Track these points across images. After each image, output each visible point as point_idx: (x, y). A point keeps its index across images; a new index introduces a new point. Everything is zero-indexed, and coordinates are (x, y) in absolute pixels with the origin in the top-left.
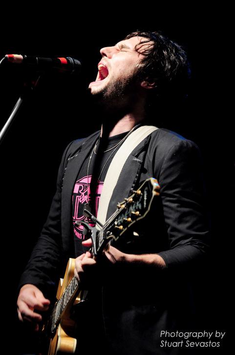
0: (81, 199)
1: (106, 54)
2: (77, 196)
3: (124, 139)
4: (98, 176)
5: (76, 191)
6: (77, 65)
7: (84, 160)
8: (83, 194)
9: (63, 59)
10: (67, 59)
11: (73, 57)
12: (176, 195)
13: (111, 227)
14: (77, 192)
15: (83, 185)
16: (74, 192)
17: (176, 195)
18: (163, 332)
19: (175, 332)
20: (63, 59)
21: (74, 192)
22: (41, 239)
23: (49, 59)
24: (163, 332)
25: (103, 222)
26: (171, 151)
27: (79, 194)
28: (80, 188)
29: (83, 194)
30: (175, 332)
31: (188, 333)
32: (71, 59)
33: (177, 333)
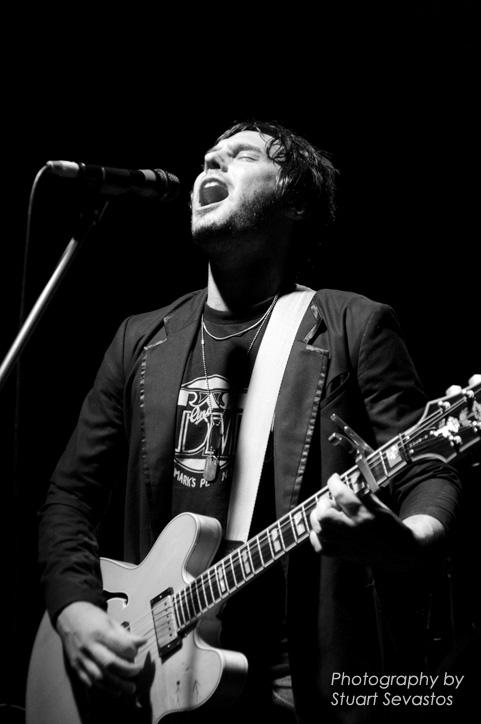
0: (192, 416)
1: (221, 164)
2: (185, 412)
3: (268, 311)
4: (238, 370)
5: (182, 400)
6: (174, 182)
7: (188, 356)
8: (197, 407)
9: (148, 173)
10: (156, 173)
11: (168, 170)
12: (85, 478)
13: (420, 440)
14: (185, 405)
15: (198, 393)
16: (180, 403)
17: (85, 478)
18: (336, 676)
19: (362, 675)
20: (148, 173)
21: (180, 403)
22: (49, 505)
23: (126, 172)
24: (336, 676)
25: (60, 496)
26: (369, 322)
27: (189, 408)
28: (191, 397)
29: (197, 407)
30: (362, 675)
31: (389, 678)
32: (163, 173)
33: (366, 676)
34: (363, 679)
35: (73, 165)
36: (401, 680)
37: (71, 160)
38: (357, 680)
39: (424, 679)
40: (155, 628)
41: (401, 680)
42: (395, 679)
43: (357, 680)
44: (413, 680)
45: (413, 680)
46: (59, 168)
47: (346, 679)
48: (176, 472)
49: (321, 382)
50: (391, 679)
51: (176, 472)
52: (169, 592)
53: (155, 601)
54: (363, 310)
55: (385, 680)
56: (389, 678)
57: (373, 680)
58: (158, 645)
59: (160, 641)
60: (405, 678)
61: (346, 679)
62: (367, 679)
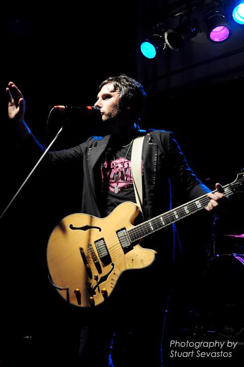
20: (102, 192)
24: (173, 342)
31: (199, 343)
33: (188, 342)
34: (186, 344)
35: (63, 107)
36: (206, 344)
37: (63, 105)
38: (183, 344)
39: (217, 344)
40: (120, 243)
41: (206, 344)
42: (202, 344)
43: (183, 344)
44: (212, 344)
45: (212, 344)
46: (59, 108)
47: (178, 344)
48: (110, 187)
49: (156, 154)
50: (200, 344)
51: (110, 187)
52: (124, 229)
53: (117, 232)
54: (158, 134)
55: (197, 344)
56: (199, 343)
57: (191, 344)
58: (123, 248)
59: (123, 245)
60: (208, 343)
61: (178, 344)
62: (188, 344)
